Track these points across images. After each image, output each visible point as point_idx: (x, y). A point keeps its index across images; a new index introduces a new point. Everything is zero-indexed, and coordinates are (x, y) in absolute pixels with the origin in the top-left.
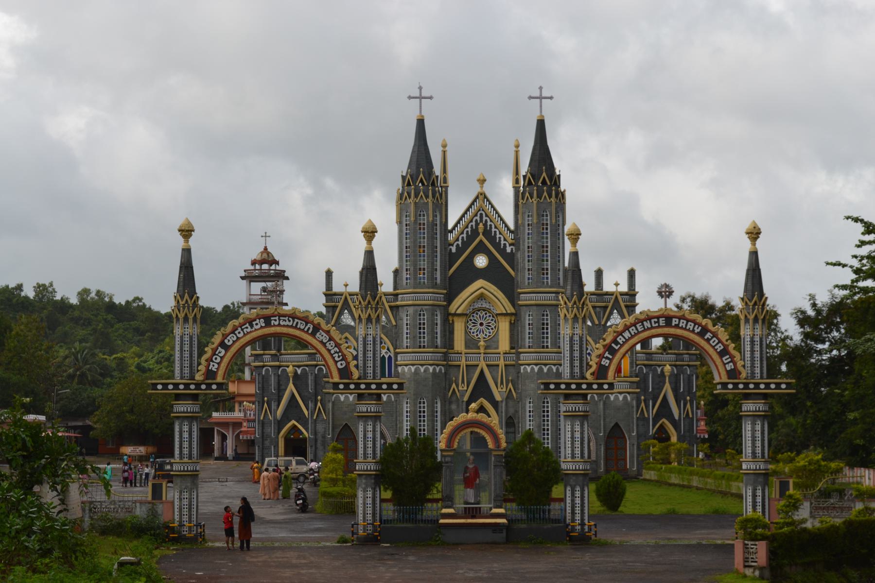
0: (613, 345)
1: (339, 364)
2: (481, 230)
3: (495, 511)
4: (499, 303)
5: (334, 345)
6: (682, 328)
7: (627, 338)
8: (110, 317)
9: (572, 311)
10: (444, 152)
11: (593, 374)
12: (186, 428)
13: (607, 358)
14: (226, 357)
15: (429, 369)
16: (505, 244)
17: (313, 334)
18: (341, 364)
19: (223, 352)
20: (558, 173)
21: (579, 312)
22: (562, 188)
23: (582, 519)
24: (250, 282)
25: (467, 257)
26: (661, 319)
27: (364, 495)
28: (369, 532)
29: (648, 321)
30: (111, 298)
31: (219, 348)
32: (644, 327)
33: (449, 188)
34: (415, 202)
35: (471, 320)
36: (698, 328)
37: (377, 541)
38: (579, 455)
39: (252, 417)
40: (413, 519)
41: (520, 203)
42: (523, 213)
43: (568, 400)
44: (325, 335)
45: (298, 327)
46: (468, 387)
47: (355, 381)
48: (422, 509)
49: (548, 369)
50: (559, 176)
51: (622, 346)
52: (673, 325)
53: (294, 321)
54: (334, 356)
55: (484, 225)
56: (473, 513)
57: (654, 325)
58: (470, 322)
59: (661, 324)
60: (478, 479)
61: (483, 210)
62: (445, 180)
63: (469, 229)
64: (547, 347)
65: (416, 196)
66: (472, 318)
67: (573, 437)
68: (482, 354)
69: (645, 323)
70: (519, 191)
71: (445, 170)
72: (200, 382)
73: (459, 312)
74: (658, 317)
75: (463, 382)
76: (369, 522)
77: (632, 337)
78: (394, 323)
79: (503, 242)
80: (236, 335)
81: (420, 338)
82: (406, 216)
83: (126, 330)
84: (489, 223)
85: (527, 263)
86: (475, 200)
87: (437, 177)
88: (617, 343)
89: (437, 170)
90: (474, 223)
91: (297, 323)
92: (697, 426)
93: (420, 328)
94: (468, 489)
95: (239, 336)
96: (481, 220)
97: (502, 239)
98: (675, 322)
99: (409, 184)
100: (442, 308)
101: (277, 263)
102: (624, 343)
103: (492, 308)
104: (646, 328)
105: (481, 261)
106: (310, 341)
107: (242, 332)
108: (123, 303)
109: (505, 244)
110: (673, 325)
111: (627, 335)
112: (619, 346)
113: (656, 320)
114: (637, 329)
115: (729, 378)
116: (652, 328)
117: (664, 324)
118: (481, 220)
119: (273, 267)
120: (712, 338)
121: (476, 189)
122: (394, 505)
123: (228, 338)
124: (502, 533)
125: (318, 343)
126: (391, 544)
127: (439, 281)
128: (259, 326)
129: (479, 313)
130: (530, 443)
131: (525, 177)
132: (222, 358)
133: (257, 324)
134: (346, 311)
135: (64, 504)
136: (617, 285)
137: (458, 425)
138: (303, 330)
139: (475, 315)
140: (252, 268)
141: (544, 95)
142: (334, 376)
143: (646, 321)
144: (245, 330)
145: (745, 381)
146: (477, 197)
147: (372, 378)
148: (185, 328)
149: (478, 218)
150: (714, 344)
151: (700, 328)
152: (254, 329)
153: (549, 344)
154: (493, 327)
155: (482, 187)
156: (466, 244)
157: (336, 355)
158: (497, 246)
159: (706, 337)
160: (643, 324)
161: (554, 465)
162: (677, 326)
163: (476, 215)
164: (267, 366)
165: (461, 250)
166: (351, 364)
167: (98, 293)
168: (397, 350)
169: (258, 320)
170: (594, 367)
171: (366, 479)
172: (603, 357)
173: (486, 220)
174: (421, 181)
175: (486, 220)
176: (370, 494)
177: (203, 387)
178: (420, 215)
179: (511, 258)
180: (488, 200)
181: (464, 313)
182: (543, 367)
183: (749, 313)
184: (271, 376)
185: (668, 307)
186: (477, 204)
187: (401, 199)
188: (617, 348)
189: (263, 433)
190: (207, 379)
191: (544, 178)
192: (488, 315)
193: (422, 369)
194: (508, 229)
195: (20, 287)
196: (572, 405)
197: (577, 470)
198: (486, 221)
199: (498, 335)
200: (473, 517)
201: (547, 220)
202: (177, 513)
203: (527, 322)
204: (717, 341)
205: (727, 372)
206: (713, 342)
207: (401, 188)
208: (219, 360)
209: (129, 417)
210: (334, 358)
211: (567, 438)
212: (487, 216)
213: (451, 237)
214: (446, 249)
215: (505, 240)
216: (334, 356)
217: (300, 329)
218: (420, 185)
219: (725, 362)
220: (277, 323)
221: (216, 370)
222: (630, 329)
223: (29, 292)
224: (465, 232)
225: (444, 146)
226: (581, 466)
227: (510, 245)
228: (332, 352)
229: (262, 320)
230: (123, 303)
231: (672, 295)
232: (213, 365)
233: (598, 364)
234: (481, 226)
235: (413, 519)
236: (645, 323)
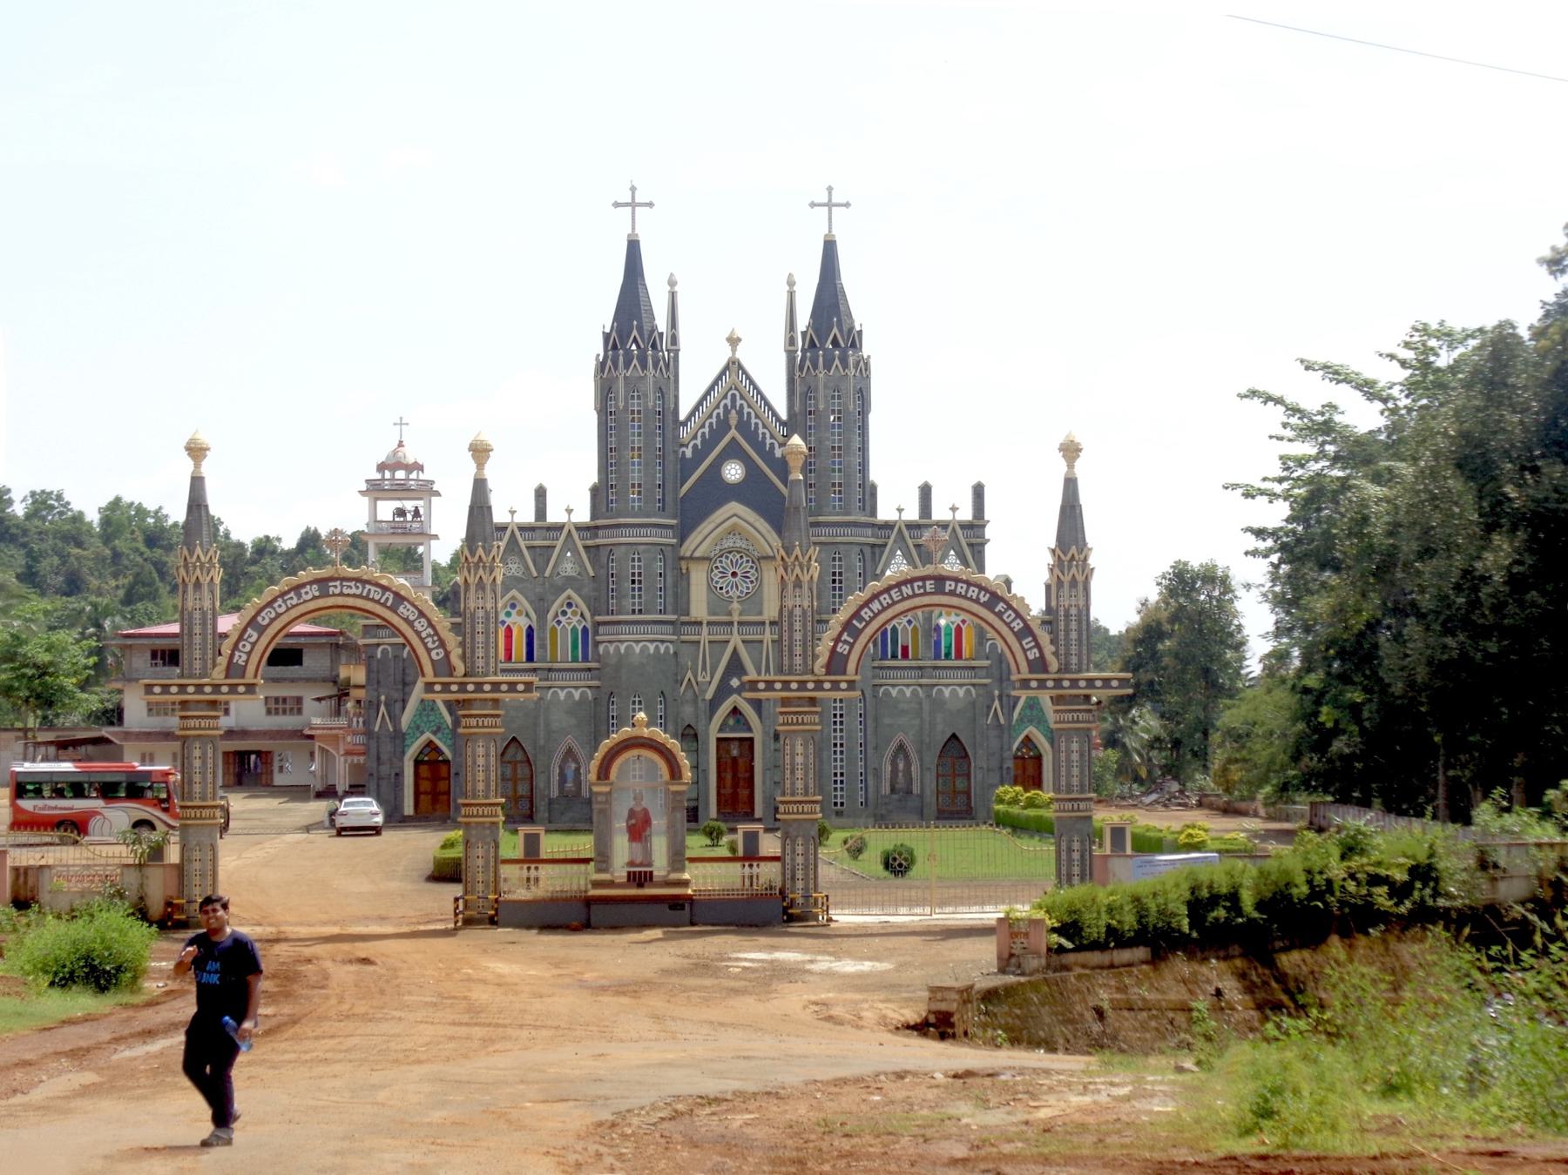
0: (855, 622)
4: (762, 540)
6: (960, 596)
10: (673, 295)
13: (846, 642)
15: (648, 648)
16: (772, 444)
20: (858, 328)
22: (865, 352)
26: (928, 583)
33: (680, 353)
34: (625, 377)
44: (412, 609)
46: (712, 678)
50: (860, 333)
51: (868, 623)
55: (737, 413)
58: (716, 571)
59: (928, 590)
61: (736, 389)
62: (674, 340)
65: (627, 365)
68: (705, 629)
69: (903, 588)
73: (697, 554)
75: (704, 668)
77: (884, 609)
79: (768, 441)
84: (746, 410)
88: (861, 619)
89: (662, 324)
90: (721, 410)
93: (633, 582)
96: (733, 406)
97: (768, 436)
99: (615, 347)
101: (420, 468)
102: (872, 619)
109: (772, 444)
111: (876, 606)
115: (1031, 671)
116: (915, 595)
118: (733, 406)
119: (413, 476)
120: (1006, 610)
121: (724, 354)
123: (263, 614)
125: (402, 621)
129: (731, 556)
131: (804, 334)
132: (254, 645)
133: (307, 593)
135: (1395, 990)
136: (954, 509)
138: (378, 602)
139: (723, 559)
140: (379, 476)
141: (834, 200)
145: (1056, 676)
146: (727, 368)
149: (728, 401)
150: (1008, 620)
155: (734, 351)
156: (709, 444)
157: (430, 639)
158: (759, 446)
160: (900, 591)
163: (725, 397)
165: (700, 455)
173: (741, 405)
174: (635, 340)
175: (741, 405)
180: (744, 372)
186: (727, 378)
188: (860, 626)
192: (745, 559)
193: (637, 648)
194: (778, 419)
199: (762, 593)
200: (640, 885)
210: (425, 645)
212: (742, 397)
213: (684, 433)
215: (772, 437)
217: (373, 600)
218: (634, 347)
224: (707, 424)
228: (424, 635)
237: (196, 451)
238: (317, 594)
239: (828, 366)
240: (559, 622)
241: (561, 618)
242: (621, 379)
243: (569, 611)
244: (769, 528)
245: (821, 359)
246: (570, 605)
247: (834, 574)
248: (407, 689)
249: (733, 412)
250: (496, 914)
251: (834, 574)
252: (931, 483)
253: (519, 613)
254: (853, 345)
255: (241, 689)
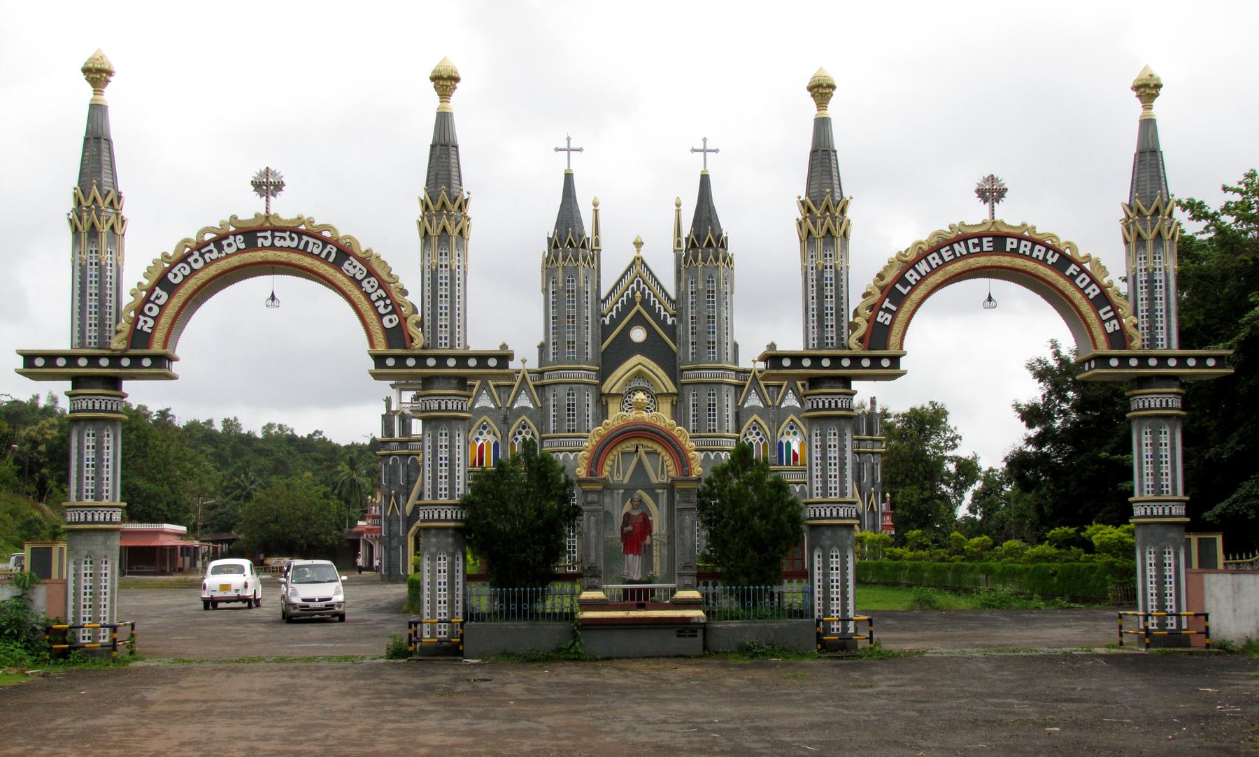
0: (898, 286)
1: (386, 320)
2: (638, 300)
3: (681, 594)
5: (376, 285)
6: (1023, 255)
7: (924, 274)
8: (292, 449)
9: (822, 225)
11: (861, 340)
12: (89, 441)
13: (887, 310)
14: (170, 306)
16: (665, 316)
17: (337, 264)
18: (391, 321)
19: (165, 296)
20: (724, 235)
21: (835, 226)
22: (730, 251)
23: (844, 609)
24: (401, 390)
25: (622, 330)
26: (985, 240)
27: (433, 568)
28: (442, 636)
29: (962, 243)
30: (292, 431)
31: (157, 288)
32: (954, 253)
34: (563, 266)
35: (627, 401)
36: (1053, 256)
37: (461, 653)
38: (838, 491)
39: (378, 513)
40: (525, 612)
41: (682, 268)
42: (686, 280)
43: (816, 388)
44: (359, 265)
45: (309, 250)
47: (417, 352)
48: (543, 592)
49: (715, 456)
50: (726, 238)
51: (914, 288)
52: (1008, 249)
53: (300, 239)
54: (377, 304)
56: (639, 598)
57: (972, 250)
58: (626, 404)
59: (985, 249)
60: (648, 537)
61: (640, 277)
63: (625, 298)
64: (714, 431)
65: (564, 259)
66: (628, 399)
67: (824, 457)
69: (956, 246)
70: (681, 255)
71: (597, 232)
72: (118, 353)
73: (613, 391)
74: (980, 237)
76: (442, 617)
77: (933, 271)
78: (540, 405)
79: (663, 313)
80: (189, 264)
81: (569, 420)
82: (553, 283)
83: (306, 459)
84: (647, 291)
85: (690, 336)
86: (631, 266)
87: (588, 239)
88: (905, 283)
89: (588, 231)
90: (630, 292)
91: (307, 242)
92: (882, 521)
93: (569, 410)
94: (631, 556)
95: (196, 266)
98: (1010, 244)
100: (595, 387)
103: (651, 387)
104: (958, 255)
105: (638, 335)
106: (330, 277)
107: (200, 260)
108: (305, 436)
109: (665, 316)
110: (1008, 249)
111: (923, 267)
112: (909, 288)
113: (976, 241)
114: (941, 257)
115: (1112, 348)
116: (969, 255)
117: (991, 249)
120: (1079, 274)
121: (632, 253)
122: (492, 585)
123: (175, 270)
124: (696, 636)
125: (346, 281)
126: (483, 659)
127: (590, 356)
128: (233, 249)
130: (744, 469)
132: (162, 307)
133: (230, 245)
134: (484, 392)
137: (610, 434)
142: (376, 342)
143: (958, 242)
144: (207, 256)
145: (1141, 352)
146: (634, 263)
147: (448, 346)
148: (91, 252)
149: (635, 285)
151: (1057, 256)
152: (224, 254)
153: (716, 428)
154: (652, 409)
155: (638, 251)
156: (621, 315)
157: (381, 303)
158: (656, 317)
159: (1068, 273)
160: (952, 249)
161: (790, 509)
162: (1014, 252)
164: (394, 454)
165: (615, 322)
166: (409, 320)
167: (280, 427)
168: (543, 435)
169: (232, 238)
170: (863, 328)
171: (436, 536)
172: (881, 309)
175: (644, 289)
176: (443, 565)
177: (126, 362)
178: (568, 281)
179: (671, 331)
181: (620, 392)
182: (710, 453)
183: (1145, 230)
184: (399, 466)
185: (997, 218)
187: (547, 263)
188: (905, 291)
189: (390, 531)
190: (132, 345)
191: (710, 239)
194: (669, 298)
195: (210, 422)
196: (823, 397)
197: (835, 518)
198: (644, 289)
200: (641, 607)
201: (713, 287)
202: (70, 610)
203: (691, 403)
204: (1088, 280)
205: (1108, 335)
206: (1082, 282)
207: (547, 252)
208: (156, 311)
209: (273, 527)
210: (376, 309)
211: (814, 459)
214: (598, 321)
216: (377, 304)
217: (311, 254)
219: (1104, 317)
220: (268, 243)
221: (150, 331)
222: (930, 258)
223: (219, 427)
224: (620, 301)
225: (595, 205)
226: (841, 510)
227: (671, 316)
228: (374, 297)
229: (240, 237)
230: (305, 436)
231: (1003, 196)
232: (145, 322)
233: (872, 322)
234: (638, 294)
235: (525, 612)
236: (956, 246)
237: (97, 75)
238: (242, 246)
239: (705, 260)
240: (516, 439)
241: (518, 436)
242: (560, 269)
243: (524, 431)
244: (664, 374)
245: (700, 254)
246: (524, 427)
247: (710, 405)
248: (410, 486)
249: (638, 292)
250: (462, 643)
251: (710, 405)
252: (776, 343)
253: (489, 433)
254: (722, 246)
255: (147, 362)
